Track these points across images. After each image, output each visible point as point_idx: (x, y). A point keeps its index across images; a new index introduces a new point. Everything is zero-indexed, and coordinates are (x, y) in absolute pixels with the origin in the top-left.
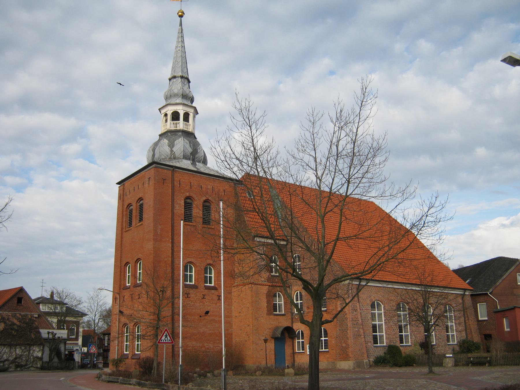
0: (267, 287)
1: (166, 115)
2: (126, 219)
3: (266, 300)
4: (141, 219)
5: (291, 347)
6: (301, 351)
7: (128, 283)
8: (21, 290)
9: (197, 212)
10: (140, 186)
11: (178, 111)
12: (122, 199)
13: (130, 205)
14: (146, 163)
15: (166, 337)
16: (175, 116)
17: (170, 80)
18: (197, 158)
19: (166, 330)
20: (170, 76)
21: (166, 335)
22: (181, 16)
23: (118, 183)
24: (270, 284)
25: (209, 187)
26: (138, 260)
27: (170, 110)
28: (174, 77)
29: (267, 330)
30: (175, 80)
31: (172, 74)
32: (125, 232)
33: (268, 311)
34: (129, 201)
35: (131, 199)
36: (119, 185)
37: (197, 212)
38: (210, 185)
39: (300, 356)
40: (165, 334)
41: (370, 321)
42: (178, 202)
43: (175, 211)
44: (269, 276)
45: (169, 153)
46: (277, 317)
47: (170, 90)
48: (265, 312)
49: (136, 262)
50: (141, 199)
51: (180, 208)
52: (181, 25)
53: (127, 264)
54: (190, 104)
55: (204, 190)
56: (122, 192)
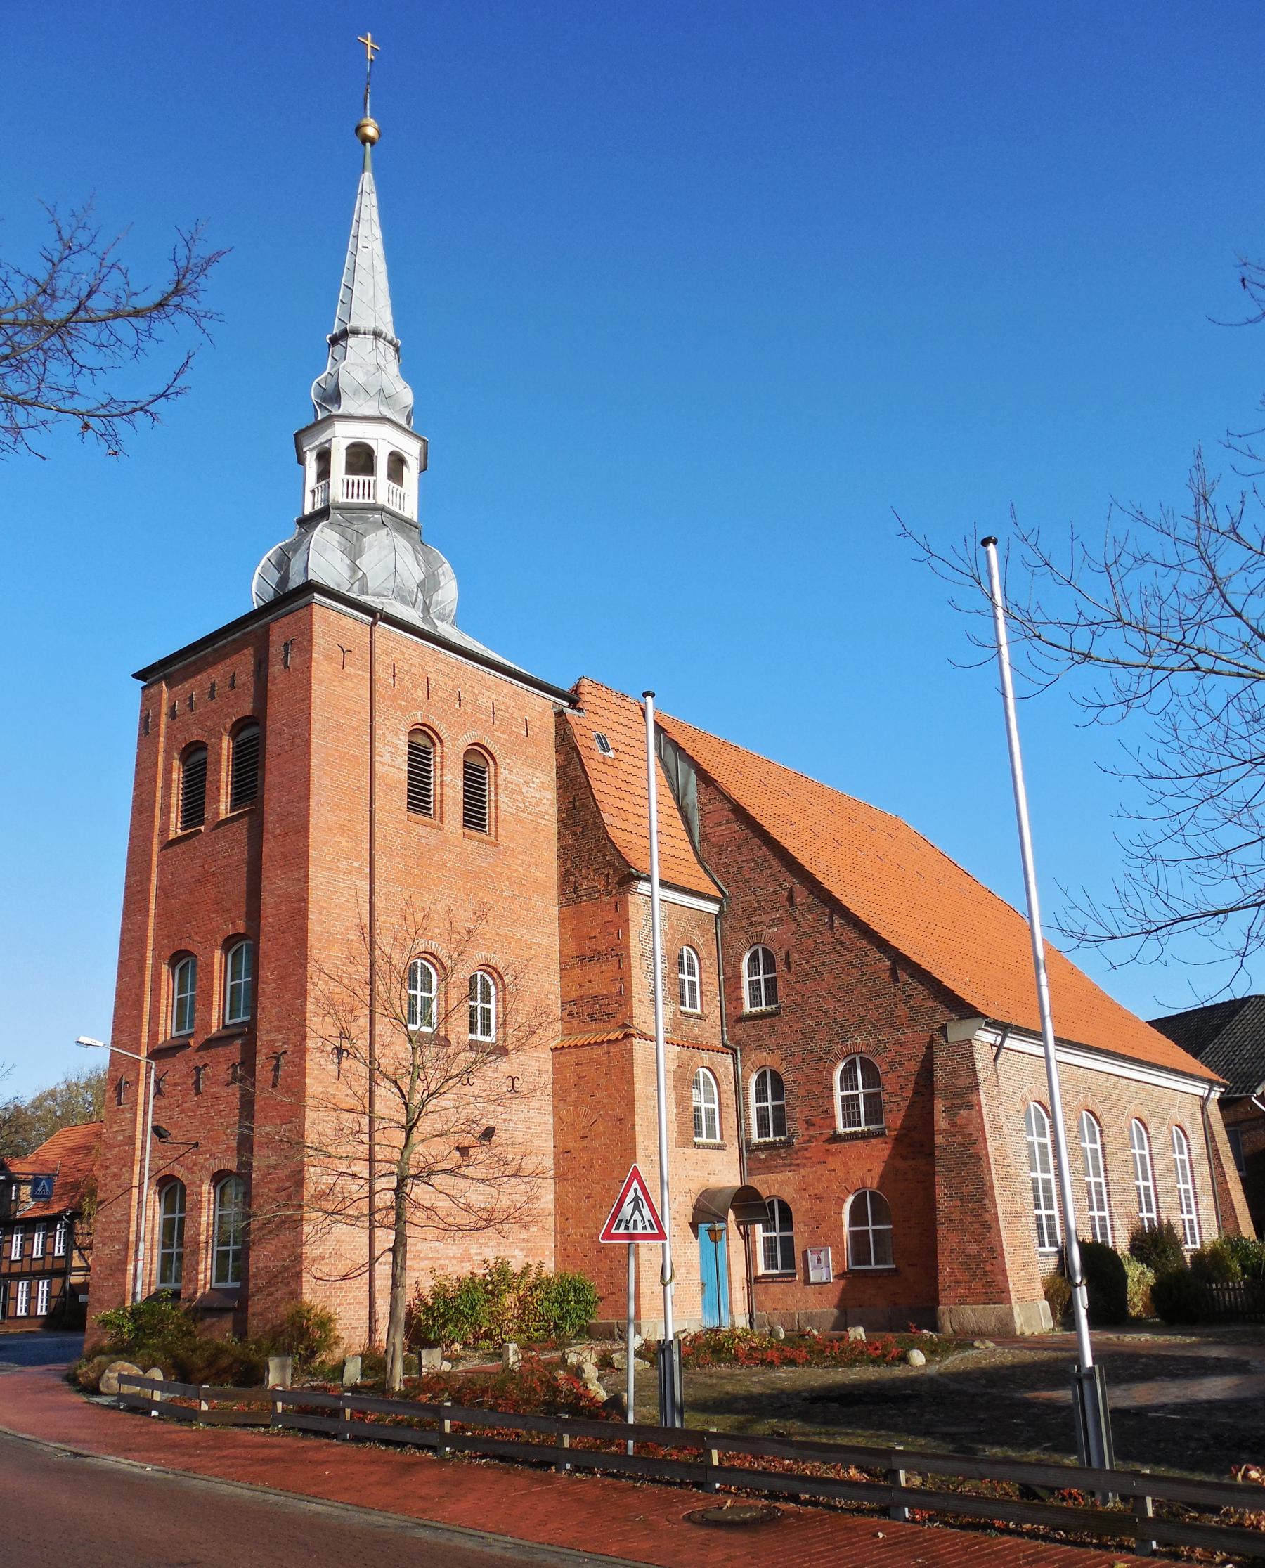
9: (449, 783)
15: (637, 1207)
18: (437, 604)
21: (636, 1199)
33: (680, 1132)
37: (449, 783)
43: (379, 768)
51: (394, 765)
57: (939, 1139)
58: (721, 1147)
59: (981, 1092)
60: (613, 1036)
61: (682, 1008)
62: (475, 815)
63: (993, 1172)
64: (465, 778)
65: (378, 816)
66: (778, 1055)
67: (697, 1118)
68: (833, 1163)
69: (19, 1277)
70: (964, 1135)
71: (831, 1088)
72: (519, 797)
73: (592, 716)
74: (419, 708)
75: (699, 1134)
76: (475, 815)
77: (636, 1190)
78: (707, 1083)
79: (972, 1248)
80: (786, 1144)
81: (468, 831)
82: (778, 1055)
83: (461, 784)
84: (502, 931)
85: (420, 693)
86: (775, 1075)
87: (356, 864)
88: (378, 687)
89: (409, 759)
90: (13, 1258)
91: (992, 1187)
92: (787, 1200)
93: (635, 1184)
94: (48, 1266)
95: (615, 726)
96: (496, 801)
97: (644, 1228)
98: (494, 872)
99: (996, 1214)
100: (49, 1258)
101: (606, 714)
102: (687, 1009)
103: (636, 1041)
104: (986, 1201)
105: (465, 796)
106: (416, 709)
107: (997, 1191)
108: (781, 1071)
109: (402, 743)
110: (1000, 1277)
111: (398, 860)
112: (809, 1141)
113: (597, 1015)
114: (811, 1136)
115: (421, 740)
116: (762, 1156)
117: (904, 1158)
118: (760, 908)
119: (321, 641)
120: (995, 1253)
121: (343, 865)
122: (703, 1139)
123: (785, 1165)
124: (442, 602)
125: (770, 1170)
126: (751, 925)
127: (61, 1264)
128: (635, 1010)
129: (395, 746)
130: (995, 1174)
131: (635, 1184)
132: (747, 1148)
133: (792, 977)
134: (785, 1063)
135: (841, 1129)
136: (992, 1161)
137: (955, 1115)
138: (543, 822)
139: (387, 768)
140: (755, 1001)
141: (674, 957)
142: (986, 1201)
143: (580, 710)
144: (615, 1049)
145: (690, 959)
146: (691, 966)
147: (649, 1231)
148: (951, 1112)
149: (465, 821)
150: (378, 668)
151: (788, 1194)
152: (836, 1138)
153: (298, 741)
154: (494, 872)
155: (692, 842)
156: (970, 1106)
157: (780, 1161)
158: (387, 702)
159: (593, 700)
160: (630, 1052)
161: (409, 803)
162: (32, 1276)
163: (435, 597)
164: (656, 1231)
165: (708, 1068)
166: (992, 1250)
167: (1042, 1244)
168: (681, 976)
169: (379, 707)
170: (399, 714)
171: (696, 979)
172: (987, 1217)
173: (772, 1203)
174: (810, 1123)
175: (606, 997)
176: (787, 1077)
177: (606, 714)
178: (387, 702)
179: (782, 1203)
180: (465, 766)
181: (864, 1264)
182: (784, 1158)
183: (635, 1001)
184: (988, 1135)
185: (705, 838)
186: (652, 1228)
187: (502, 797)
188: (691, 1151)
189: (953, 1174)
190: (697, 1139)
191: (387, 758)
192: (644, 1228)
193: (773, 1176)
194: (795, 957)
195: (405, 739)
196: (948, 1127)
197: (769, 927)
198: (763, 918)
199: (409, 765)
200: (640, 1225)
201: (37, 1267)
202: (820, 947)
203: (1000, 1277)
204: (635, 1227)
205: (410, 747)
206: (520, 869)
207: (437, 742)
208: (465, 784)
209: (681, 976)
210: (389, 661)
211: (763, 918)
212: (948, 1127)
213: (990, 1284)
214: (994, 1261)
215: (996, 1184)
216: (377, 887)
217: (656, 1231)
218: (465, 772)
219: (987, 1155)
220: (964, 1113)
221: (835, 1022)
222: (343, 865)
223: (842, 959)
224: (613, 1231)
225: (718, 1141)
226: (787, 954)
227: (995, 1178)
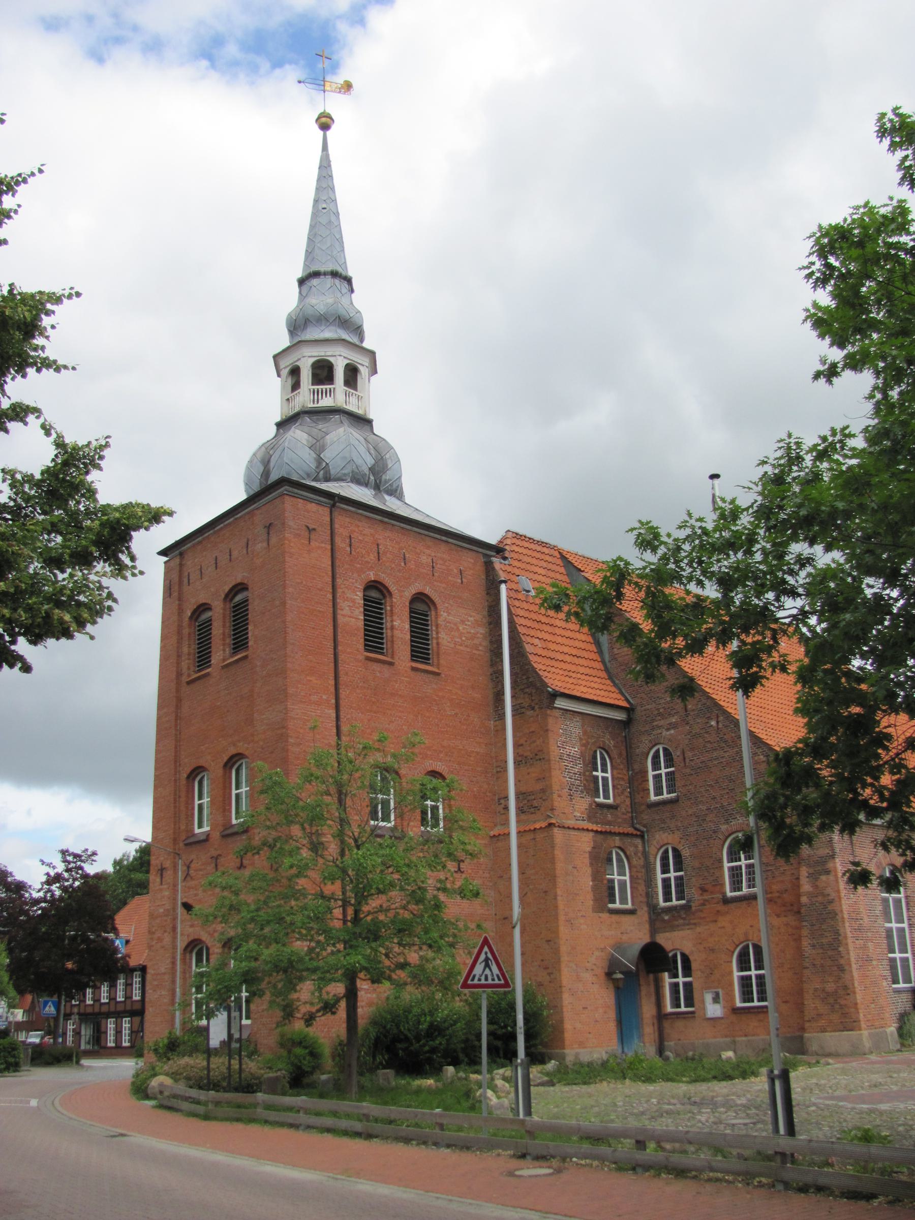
0: (591, 834)
1: (295, 372)
2: (189, 648)
3: (589, 871)
4: (240, 642)
5: (653, 999)
6: (756, 1003)
7: (200, 826)
8: (833, 241)
9: (399, 626)
10: (235, 554)
11: (332, 359)
12: (175, 594)
13: (203, 608)
14: (243, 496)
15: (487, 965)
16: (323, 373)
17: (301, 282)
18: (386, 482)
19: (486, 942)
20: (299, 274)
21: (487, 960)
22: (325, 127)
23: (163, 553)
24: (599, 828)
25: (425, 559)
26: (233, 761)
27: (306, 361)
28: (316, 274)
29: (597, 953)
30: (315, 282)
31: (305, 265)
32: (188, 683)
33: (596, 900)
34: (202, 598)
35: (210, 590)
36: (166, 559)
37: (399, 626)
38: (427, 554)
39: (680, 1024)
40: (483, 957)
41: (880, 921)
42: (349, 595)
43: (341, 620)
44: (590, 805)
45: (313, 465)
46: (615, 918)
47: (301, 308)
48: (590, 903)
49: (225, 765)
50: (240, 587)
51: (353, 614)
52: (325, 147)
53: (196, 772)
54: (358, 343)
55: (412, 565)
56: (175, 577)
57: (804, 899)
58: (631, 912)
59: (837, 860)
60: (537, 826)
61: (597, 800)
62: (421, 649)
63: (847, 924)
64: (411, 622)
65: (341, 657)
66: (678, 834)
67: (612, 889)
68: (724, 921)
69: (108, 1015)
70: (824, 895)
71: (720, 861)
72: (457, 634)
73: (516, 563)
74: (371, 569)
75: (614, 902)
76: (421, 649)
77: (486, 953)
78: (620, 860)
79: (830, 987)
80: (686, 908)
81: (415, 665)
82: (678, 834)
83: (407, 626)
84: (445, 743)
85: (372, 557)
86: (675, 850)
87: (324, 697)
88: (338, 555)
89: (365, 610)
90: (118, 1000)
91: (846, 937)
92: (687, 952)
93: (486, 949)
94: (128, 1008)
95: (536, 569)
96: (437, 638)
97: (493, 980)
98: (437, 696)
99: (849, 959)
100: (128, 1002)
101: (529, 560)
102: (601, 800)
103: (556, 830)
104: (841, 949)
105: (412, 636)
106: (369, 570)
107: (850, 941)
108: (680, 847)
109: (359, 597)
110: (853, 1010)
111: (358, 691)
112: (703, 904)
113: (525, 809)
114: (705, 900)
115: (374, 594)
116: (666, 918)
117: (778, 916)
118: (660, 714)
119: (291, 523)
120: (847, 990)
121: (314, 698)
122: (617, 905)
123: (684, 925)
124: (390, 480)
125: (673, 928)
126: (653, 729)
127: (137, 1007)
128: (556, 804)
129: (353, 601)
130: (848, 929)
131: (486, 949)
132: (655, 913)
133: (688, 771)
134: (683, 841)
135: (729, 894)
136: (846, 916)
137: (817, 879)
138: (477, 652)
139: (347, 618)
140: (659, 791)
141: (588, 758)
142: (841, 949)
143: (505, 558)
144: (540, 836)
145: (603, 759)
146: (604, 765)
147: (497, 982)
148: (814, 877)
149: (412, 656)
150: (338, 540)
151: (687, 947)
152: (726, 901)
153: (277, 603)
154: (437, 696)
155: (603, 662)
156: (828, 872)
157: (681, 921)
158: (346, 566)
159: (514, 548)
160: (552, 838)
161: (366, 645)
162: (118, 1015)
163: (384, 477)
164: (502, 982)
165: (620, 848)
166: (845, 987)
167: (895, 981)
168: (595, 773)
169: (339, 571)
170: (355, 575)
171: (609, 775)
172: (842, 961)
173: (675, 956)
174: (703, 890)
175: (532, 793)
176: (685, 853)
177: (529, 560)
178: (346, 566)
179: (684, 955)
180: (411, 612)
181: (749, 1002)
182: (684, 919)
183: (555, 796)
184: (843, 895)
185: (614, 658)
186: (499, 980)
187: (442, 635)
188: (605, 915)
189: (815, 928)
190: (610, 906)
191: (346, 611)
192: (493, 980)
193: (676, 933)
194: (689, 754)
195: (360, 594)
196: (811, 889)
197: (668, 730)
198: (662, 723)
199: (365, 615)
200: (490, 978)
201: (120, 1008)
202: (708, 745)
203: (853, 1010)
204: (486, 979)
205: (365, 600)
206: (460, 692)
207: (385, 592)
208: (411, 626)
209: (595, 773)
210: (346, 533)
211: (662, 723)
212: (811, 889)
213: (845, 1015)
214: (847, 997)
215: (849, 935)
216: (342, 714)
217: (502, 982)
218: (411, 617)
219: (842, 911)
220: (823, 878)
221: (722, 807)
222: (314, 698)
223: (726, 755)
224: (469, 982)
225: (629, 906)
226: (683, 753)
227: (848, 930)
